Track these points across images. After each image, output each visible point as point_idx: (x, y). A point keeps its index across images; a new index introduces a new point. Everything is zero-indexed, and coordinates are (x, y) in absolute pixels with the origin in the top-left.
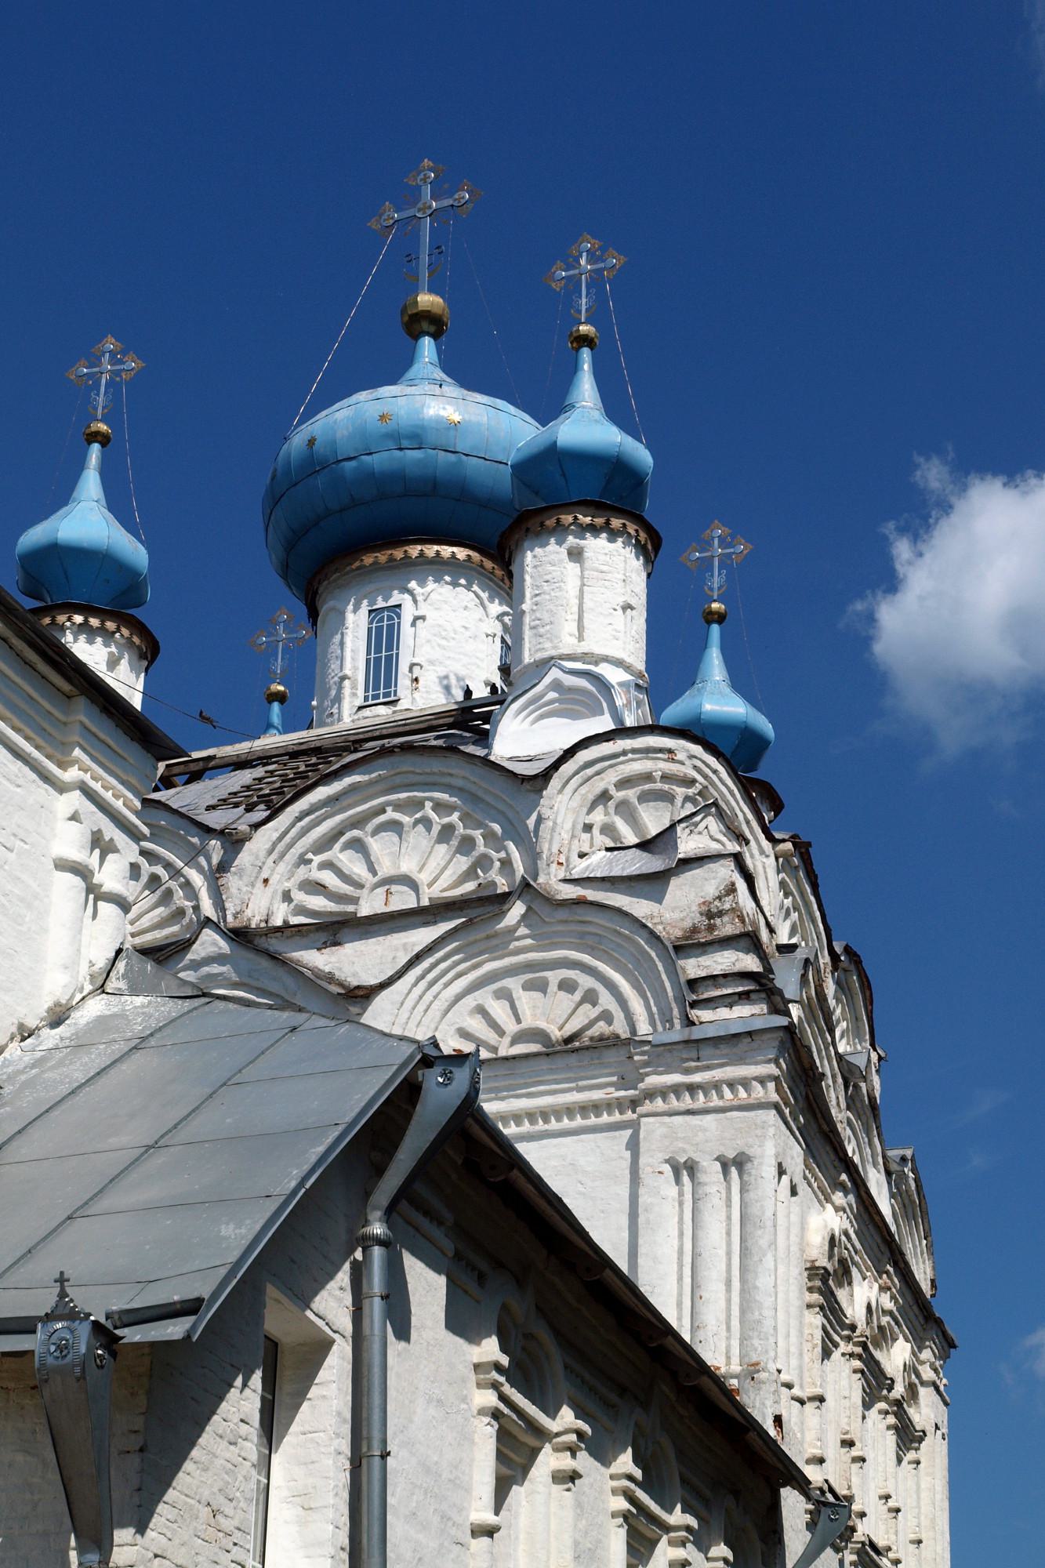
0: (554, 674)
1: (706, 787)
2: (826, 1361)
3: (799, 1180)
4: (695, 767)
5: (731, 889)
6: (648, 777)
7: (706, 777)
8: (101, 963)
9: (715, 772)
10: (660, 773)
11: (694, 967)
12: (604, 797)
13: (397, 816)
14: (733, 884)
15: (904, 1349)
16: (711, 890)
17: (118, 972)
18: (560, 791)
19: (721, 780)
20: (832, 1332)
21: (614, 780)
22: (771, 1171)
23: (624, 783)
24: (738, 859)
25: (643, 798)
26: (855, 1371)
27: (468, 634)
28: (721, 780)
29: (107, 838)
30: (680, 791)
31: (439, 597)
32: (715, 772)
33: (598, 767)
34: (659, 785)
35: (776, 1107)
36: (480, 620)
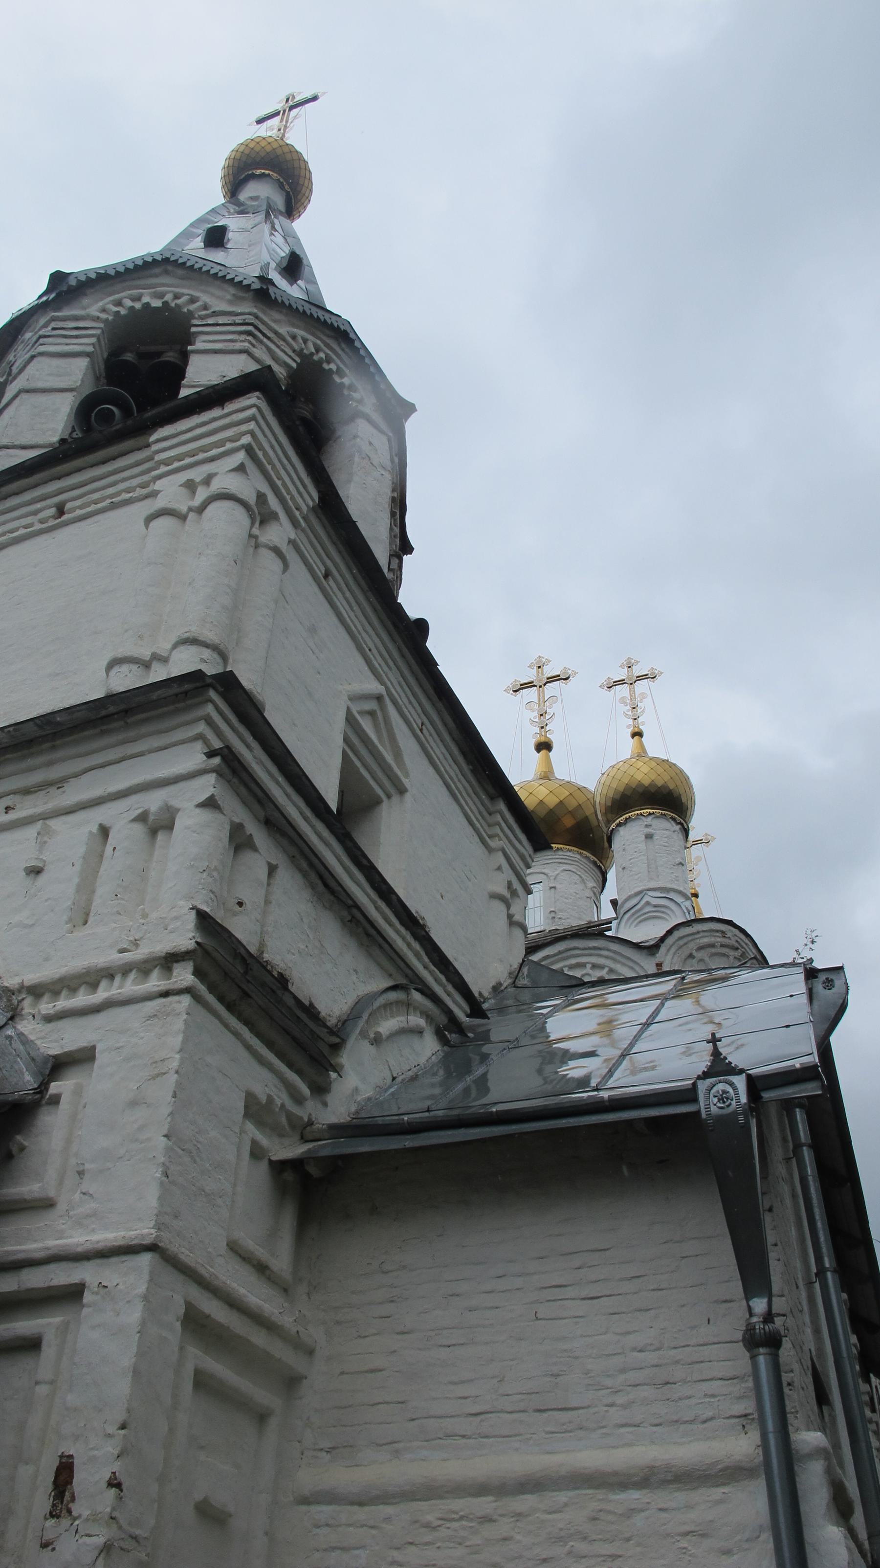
0: (646, 899)
1: (744, 952)
4: (737, 941)
6: (712, 946)
7: (743, 947)
8: (516, 966)
9: (746, 944)
12: (691, 956)
17: (523, 974)
18: (666, 954)
19: (750, 949)
23: (701, 948)
25: (713, 955)
27: (578, 896)
28: (750, 949)
29: (515, 888)
30: (732, 953)
31: (562, 878)
32: (746, 944)
33: (685, 940)
36: (583, 889)
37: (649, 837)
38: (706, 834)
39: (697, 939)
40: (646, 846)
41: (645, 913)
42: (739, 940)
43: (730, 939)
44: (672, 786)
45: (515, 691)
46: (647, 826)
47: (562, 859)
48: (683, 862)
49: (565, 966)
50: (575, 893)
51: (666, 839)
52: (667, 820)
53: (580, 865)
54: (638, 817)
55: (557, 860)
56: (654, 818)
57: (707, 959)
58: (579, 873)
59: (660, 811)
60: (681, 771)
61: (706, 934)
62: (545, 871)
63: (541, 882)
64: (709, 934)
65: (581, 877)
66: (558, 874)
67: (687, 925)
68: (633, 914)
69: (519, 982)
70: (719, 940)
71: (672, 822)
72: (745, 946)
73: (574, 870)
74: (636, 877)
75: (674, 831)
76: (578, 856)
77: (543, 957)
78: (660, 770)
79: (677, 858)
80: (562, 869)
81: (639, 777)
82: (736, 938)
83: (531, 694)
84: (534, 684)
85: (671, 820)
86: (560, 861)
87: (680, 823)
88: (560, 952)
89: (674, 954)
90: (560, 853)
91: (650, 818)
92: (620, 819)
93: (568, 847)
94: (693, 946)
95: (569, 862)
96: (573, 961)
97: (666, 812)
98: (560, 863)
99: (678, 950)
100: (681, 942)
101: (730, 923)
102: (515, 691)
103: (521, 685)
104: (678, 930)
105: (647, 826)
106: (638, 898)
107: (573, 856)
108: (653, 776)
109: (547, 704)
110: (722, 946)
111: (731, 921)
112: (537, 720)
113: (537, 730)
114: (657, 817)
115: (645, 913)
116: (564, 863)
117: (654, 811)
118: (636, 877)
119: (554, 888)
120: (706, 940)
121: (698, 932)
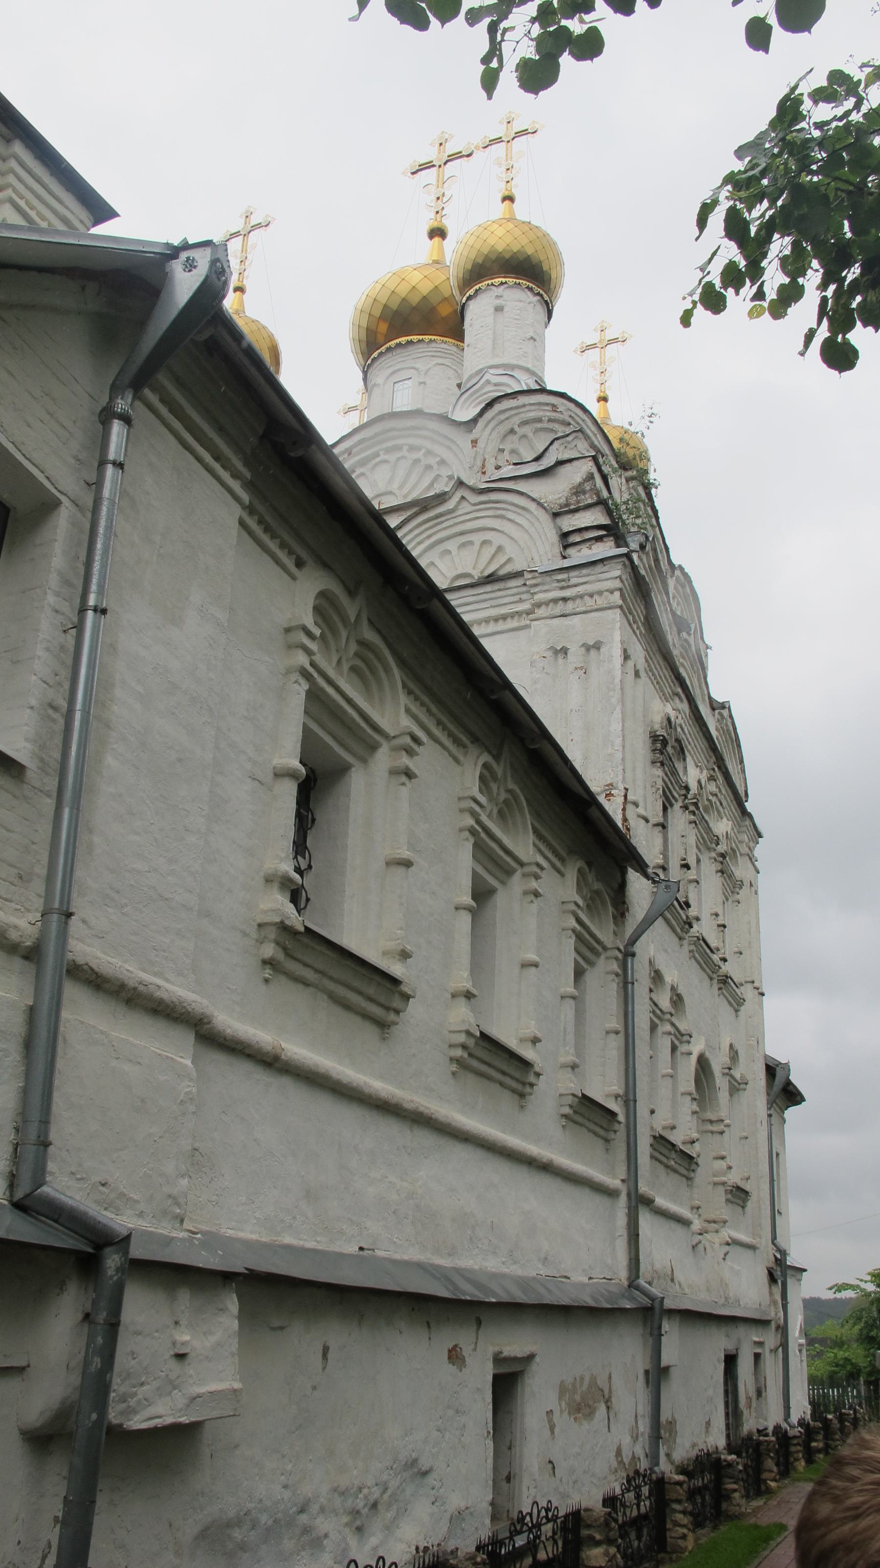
0: (487, 377)
2: (760, 1399)
3: (641, 665)
4: (570, 416)
5: (590, 477)
6: (539, 420)
9: (583, 421)
10: (547, 418)
11: (569, 523)
12: (512, 431)
13: (386, 457)
14: (592, 474)
15: (727, 825)
16: (578, 479)
19: (587, 426)
20: (672, 789)
21: (518, 422)
22: (617, 653)
24: (595, 459)
25: (537, 431)
26: (690, 823)
32: (583, 421)
33: (507, 415)
34: (545, 425)
35: (621, 607)
37: (499, 309)
38: (623, 332)
39: (522, 413)
40: (494, 319)
41: (486, 393)
42: (573, 415)
43: (562, 414)
44: (530, 251)
45: (413, 173)
46: (498, 297)
47: (435, 351)
48: (535, 337)
49: (381, 450)
50: (448, 389)
51: (519, 312)
52: (523, 290)
53: (455, 358)
54: (489, 287)
55: (430, 354)
56: (506, 288)
57: (530, 435)
58: (454, 367)
59: (514, 280)
60: (545, 235)
61: (533, 408)
62: (417, 366)
63: (410, 378)
64: (537, 407)
65: (457, 372)
66: (429, 369)
67: (511, 397)
68: (471, 395)
69: (617, 573)
70: (548, 414)
71: (529, 293)
72: (581, 422)
73: (448, 364)
74: (480, 354)
75: (529, 303)
76: (455, 349)
77: (359, 441)
78: (517, 232)
79: (529, 332)
80: (434, 363)
81: (492, 241)
82: (570, 413)
83: (429, 175)
84: (434, 163)
85: (526, 290)
86: (434, 354)
87: (538, 294)
88: (376, 435)
89: (493, 429)
90: (434, 345)
91: (502, 287)
92: (470, 292)
93: (442, 338)
94: (516, 420)
95: (443, 355)
96: (390, 444)
97: (521, 281)
98: (433, 356)
99: (497, 425)
100: (503, 417)
101: (563, 395)
102: (413, 173)
103: (420, 166)
104: (500, 403)
105: (498, 297)
106: (478, 378)
107: (448, 348)
108: (508, 239)
109: (446, 185)
110: (550, 420)
111: (565, 393)
112: (433, 204)
113: (433, 215)
114: (510, 287)
115: (486, 393)
116: (437, 356)
117: (507, 280)
118: (480, 354)
119: (424, 383)
120: (532, 415)
121: (524, 406)
